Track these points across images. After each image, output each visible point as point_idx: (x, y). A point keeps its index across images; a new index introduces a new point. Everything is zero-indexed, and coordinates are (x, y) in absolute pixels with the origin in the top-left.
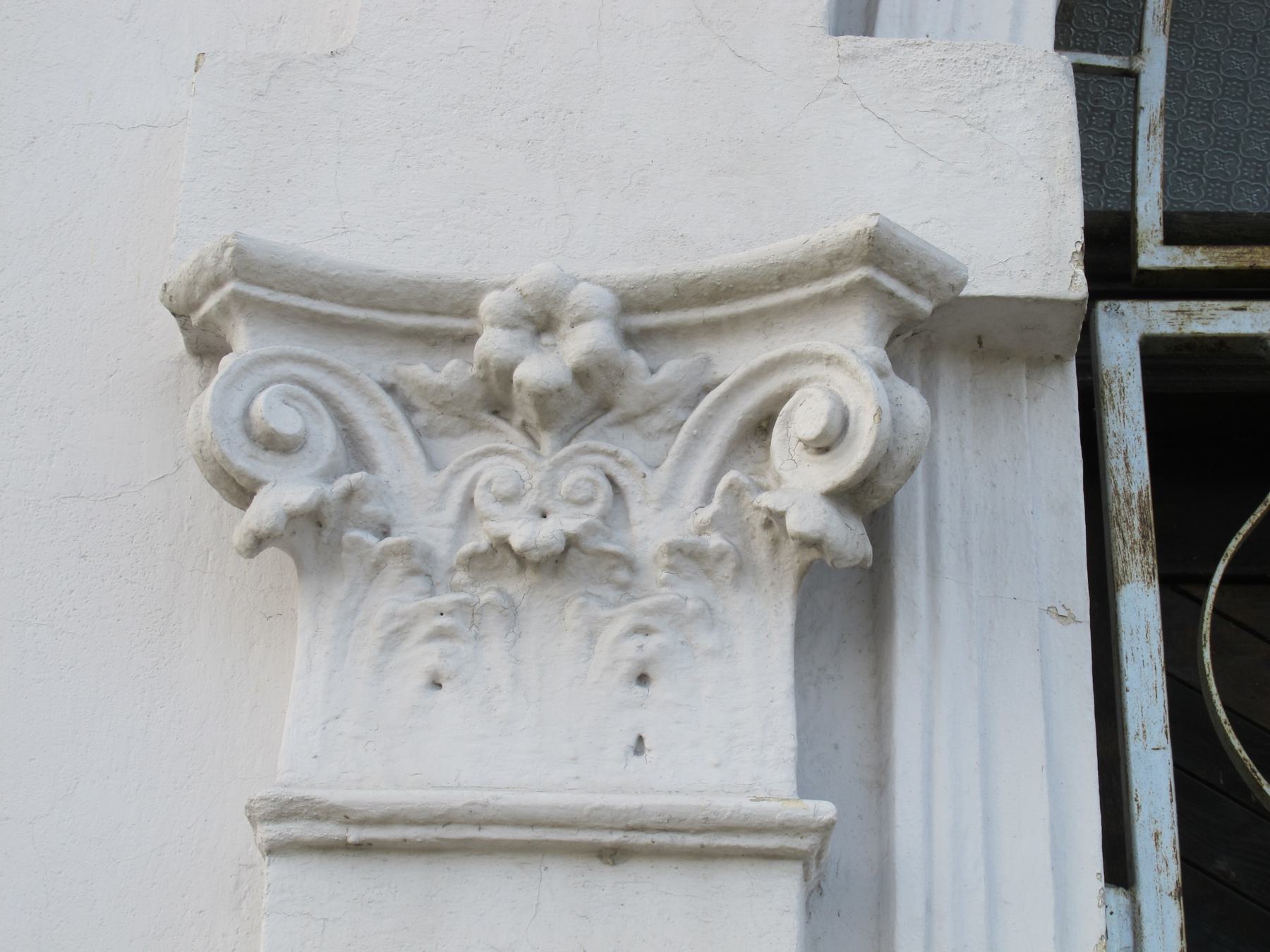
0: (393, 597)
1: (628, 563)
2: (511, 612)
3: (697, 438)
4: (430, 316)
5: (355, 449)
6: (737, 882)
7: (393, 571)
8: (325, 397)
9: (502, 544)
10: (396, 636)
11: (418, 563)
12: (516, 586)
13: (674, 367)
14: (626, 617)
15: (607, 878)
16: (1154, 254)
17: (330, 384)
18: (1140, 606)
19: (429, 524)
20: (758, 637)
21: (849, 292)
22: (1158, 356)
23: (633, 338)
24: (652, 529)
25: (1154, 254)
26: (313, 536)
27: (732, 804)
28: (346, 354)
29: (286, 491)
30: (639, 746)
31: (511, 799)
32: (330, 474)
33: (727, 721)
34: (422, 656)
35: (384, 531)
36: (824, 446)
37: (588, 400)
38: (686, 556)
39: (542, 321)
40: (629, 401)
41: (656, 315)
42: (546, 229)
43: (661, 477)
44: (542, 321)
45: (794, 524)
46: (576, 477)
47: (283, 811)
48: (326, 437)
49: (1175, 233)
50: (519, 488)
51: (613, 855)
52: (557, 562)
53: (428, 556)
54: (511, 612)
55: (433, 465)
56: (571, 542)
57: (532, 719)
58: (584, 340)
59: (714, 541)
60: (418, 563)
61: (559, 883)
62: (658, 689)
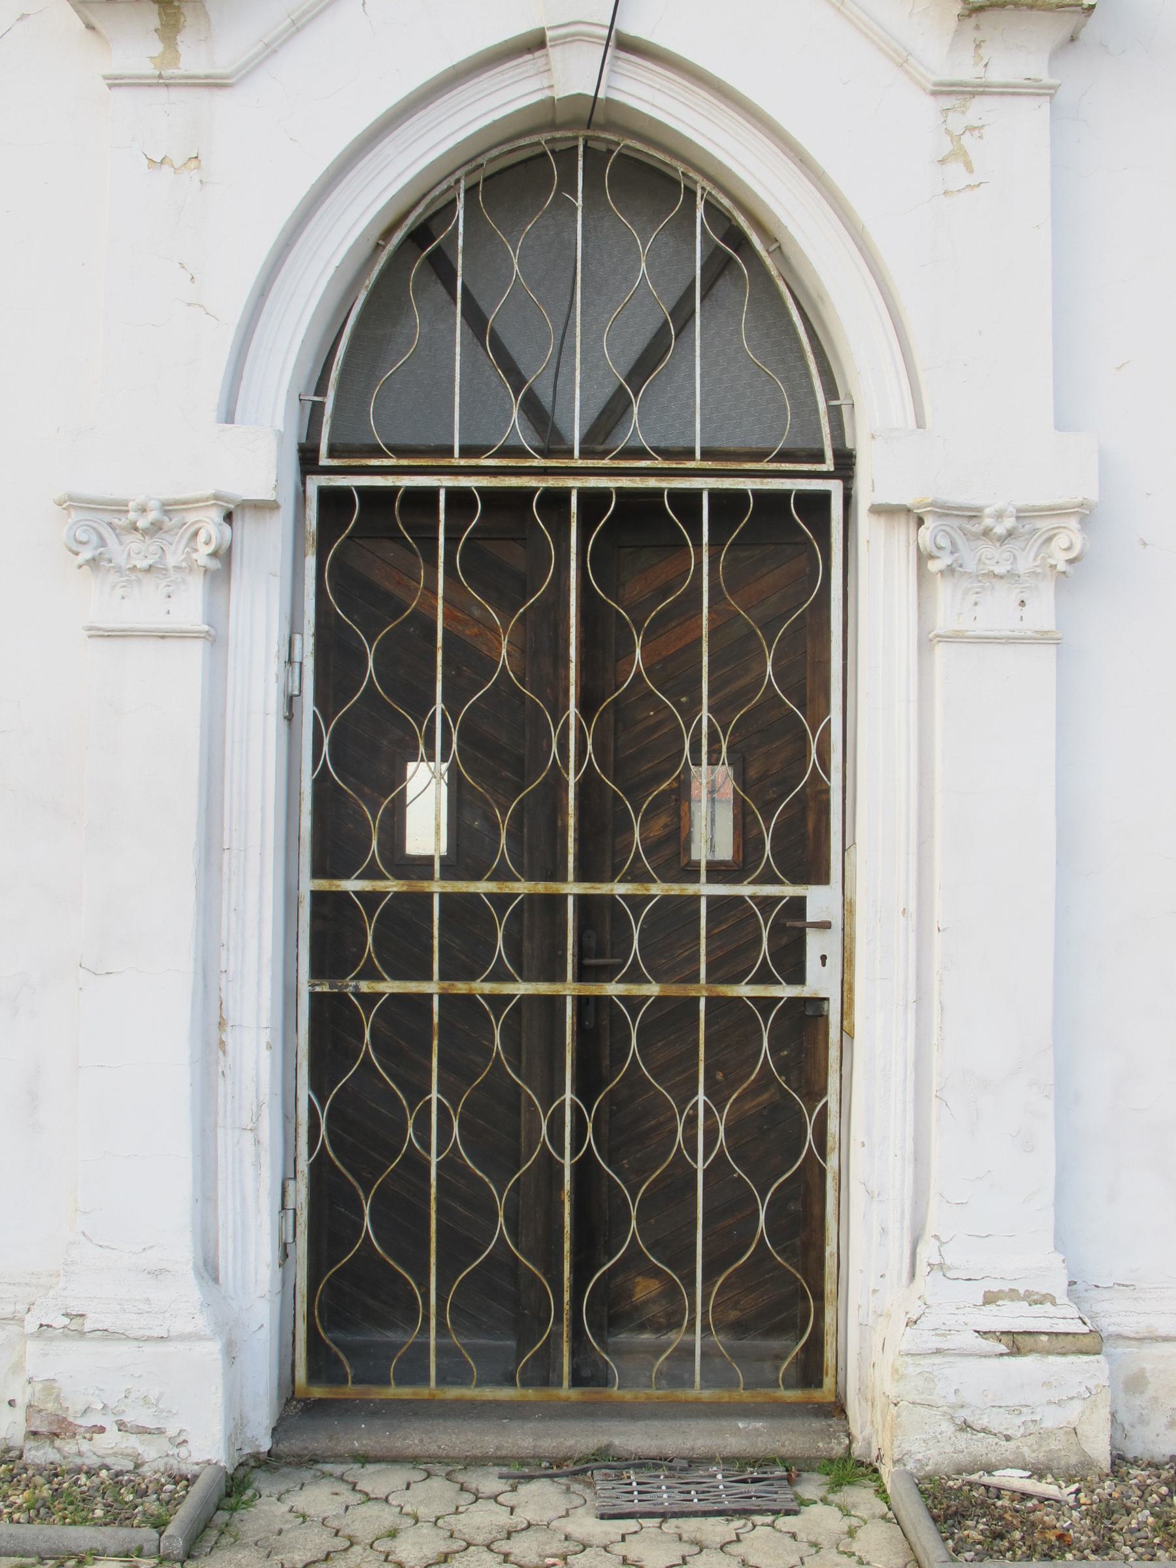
0: (113, 578)
1: (166, 569)
2: (139, 581)
3: (181, 538)
4: (120, 507)
5: (103, 542)
6: (189, 642)
7: (112, 571)
8: (94, 528)
9: (135, 566)
10: (114, 587)
11: (119, 570)
12: (140, 575)
13: (176, 520)
14: (164, 583)
15: (161, 641)
16: (324, 461)
17: (95, 525)
18: (311, 562)
19: (120, 560)
20: (196, 587)
21: (212, 505)
22: (323, 493)
23: (166, 512)
24: (172, 560)
25: (324, 461)
26: (94, 562)
27: (189, 627)
28: (100, 516)
29: (87, 554)
30: (169, 612)
31: (138, 626)
32: (96, 548)
33: (188, 605)
34: (119, 592)
35: (110, 561)
36: (207, 543)
37: (156, 528)
38: (178, 568)
39: (143, 510)
40: (165, 528)
41: (168, 508)
42: (144, 487)
43: (173, 547)
44: (143, 510)
45: (200, 563)
46: (153, 548)
47: (90, 629)
48: (95, 539)
49: (332, 453)
50: (137, 551)
51: (163, 637)
52: (149, 569)
53: (120, 567)
54: (139, 581)
55: (121, 543)
56: (150, 566)
57: (145, 606)
58: (153, 515)
59: (184, 564)
60: (119, 570)
61: (152, 643)
62: (172, 599)
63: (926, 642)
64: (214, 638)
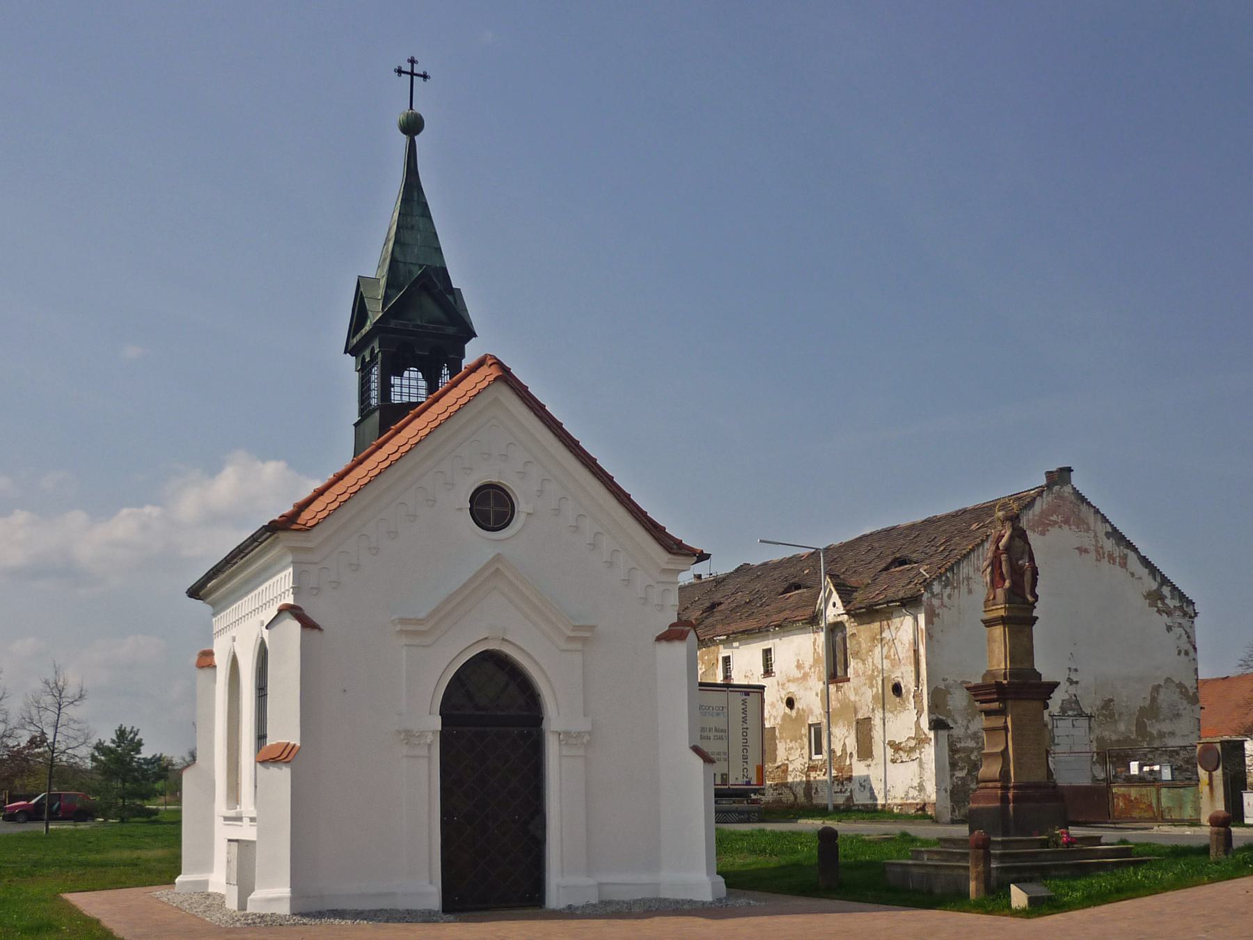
33: (425, 752)
63: (561, 756)
64: (430, 758)
